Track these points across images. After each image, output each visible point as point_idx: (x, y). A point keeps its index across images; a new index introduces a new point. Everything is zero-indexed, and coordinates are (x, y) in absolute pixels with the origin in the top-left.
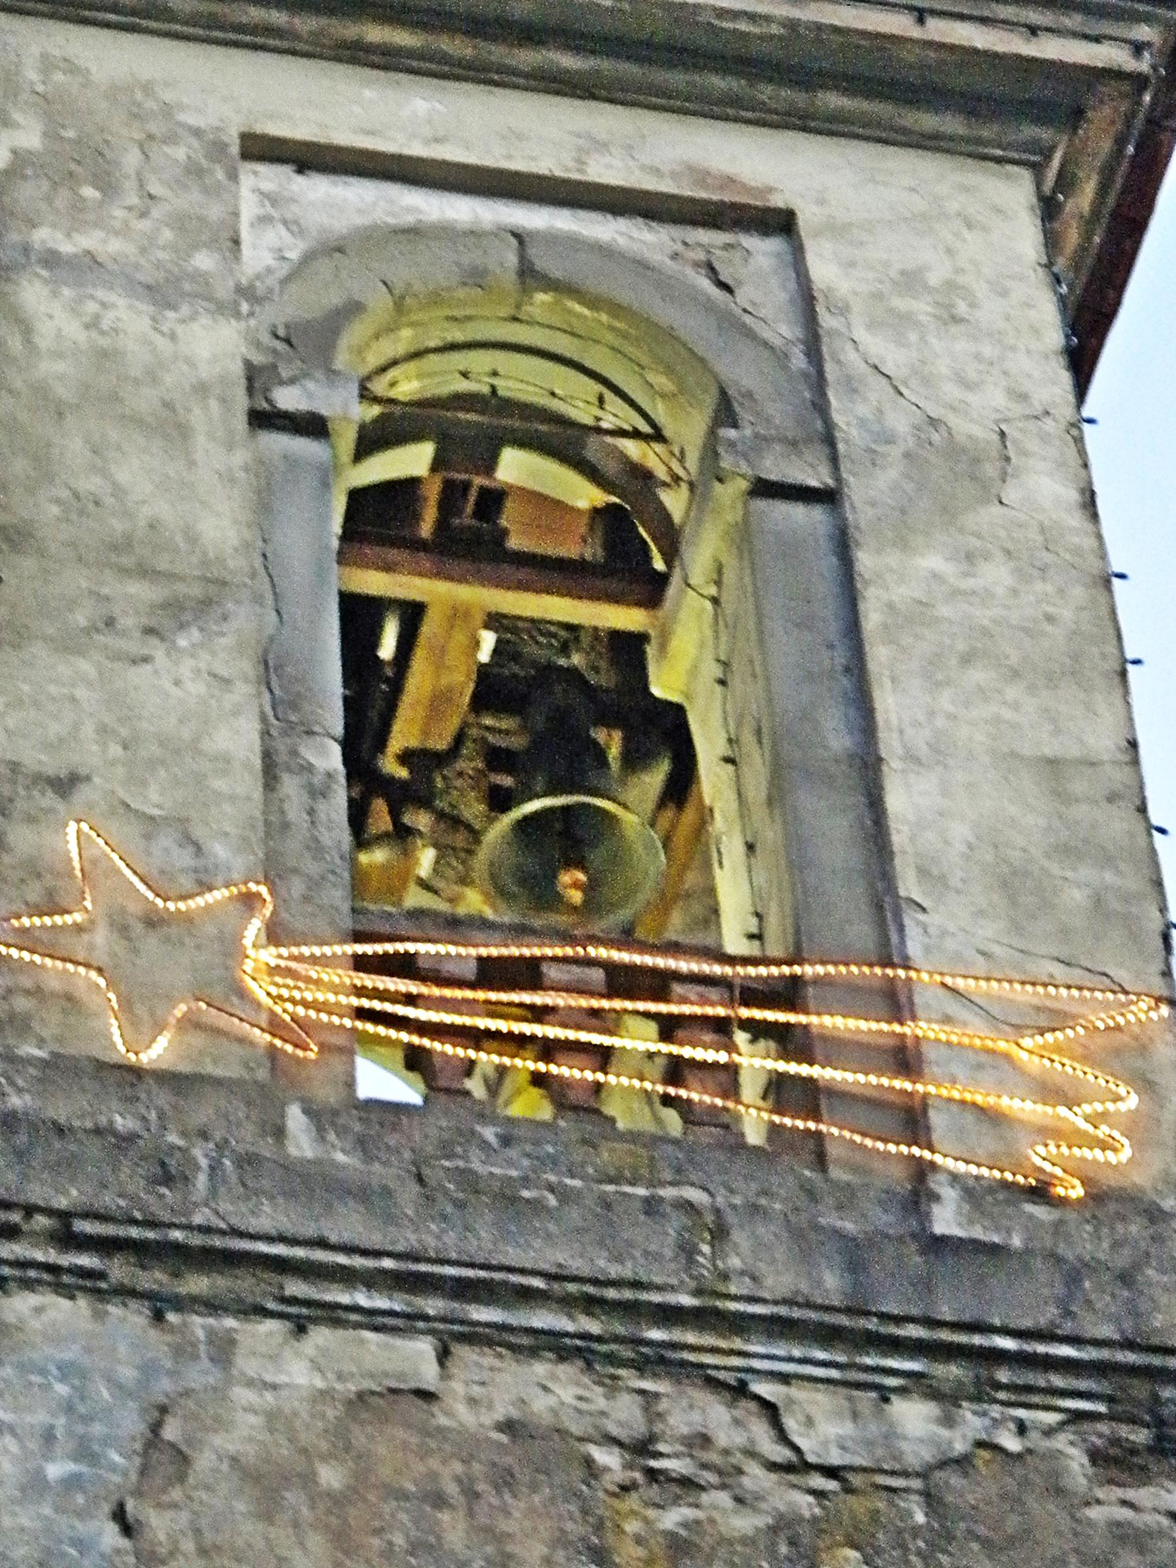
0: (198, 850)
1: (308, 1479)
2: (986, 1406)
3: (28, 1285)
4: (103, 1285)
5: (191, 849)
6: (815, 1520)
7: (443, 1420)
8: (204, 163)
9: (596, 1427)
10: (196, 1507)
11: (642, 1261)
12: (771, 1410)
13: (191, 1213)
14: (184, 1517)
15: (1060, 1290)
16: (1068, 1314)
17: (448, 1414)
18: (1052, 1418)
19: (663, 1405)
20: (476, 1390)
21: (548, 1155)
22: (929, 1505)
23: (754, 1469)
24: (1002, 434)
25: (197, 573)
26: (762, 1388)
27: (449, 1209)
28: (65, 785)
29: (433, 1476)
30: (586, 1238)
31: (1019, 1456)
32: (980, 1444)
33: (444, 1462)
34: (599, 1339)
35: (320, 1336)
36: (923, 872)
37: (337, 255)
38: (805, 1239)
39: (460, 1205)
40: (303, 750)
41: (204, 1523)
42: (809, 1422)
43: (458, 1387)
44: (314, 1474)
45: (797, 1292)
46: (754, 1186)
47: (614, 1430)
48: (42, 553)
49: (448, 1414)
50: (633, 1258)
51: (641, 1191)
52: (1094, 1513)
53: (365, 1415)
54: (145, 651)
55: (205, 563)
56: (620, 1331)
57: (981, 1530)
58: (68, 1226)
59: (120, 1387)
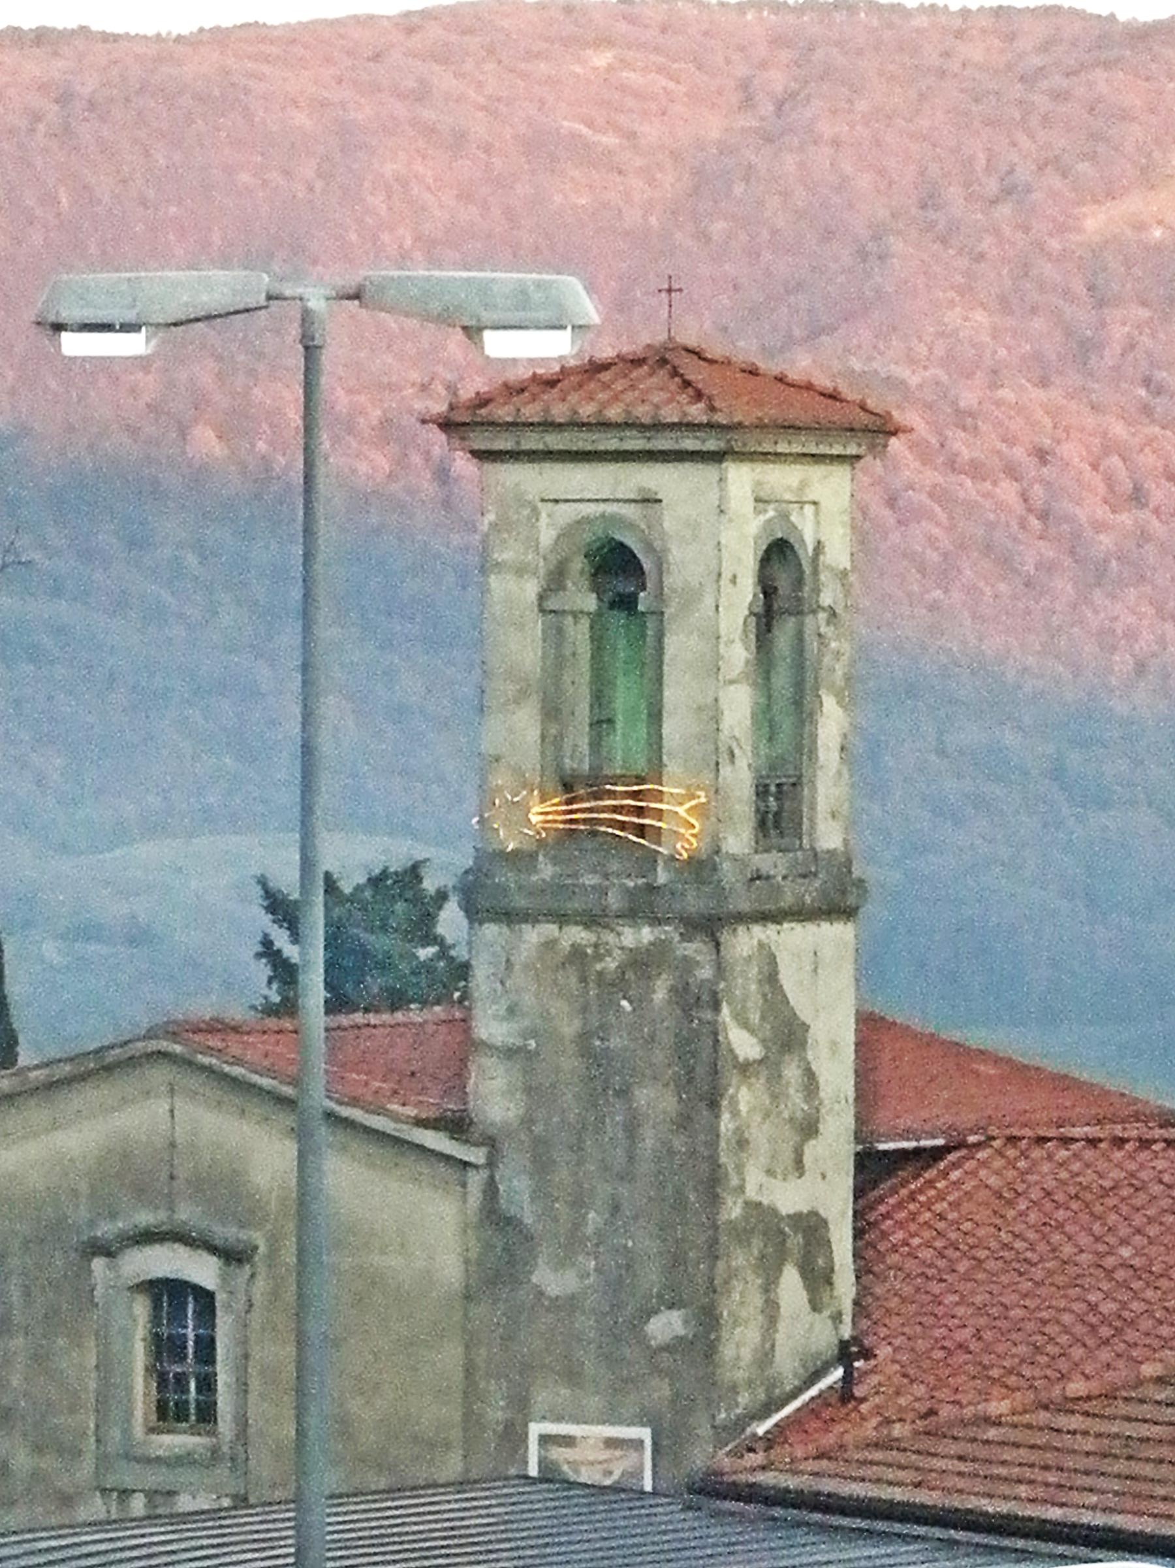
56: (591, 920)
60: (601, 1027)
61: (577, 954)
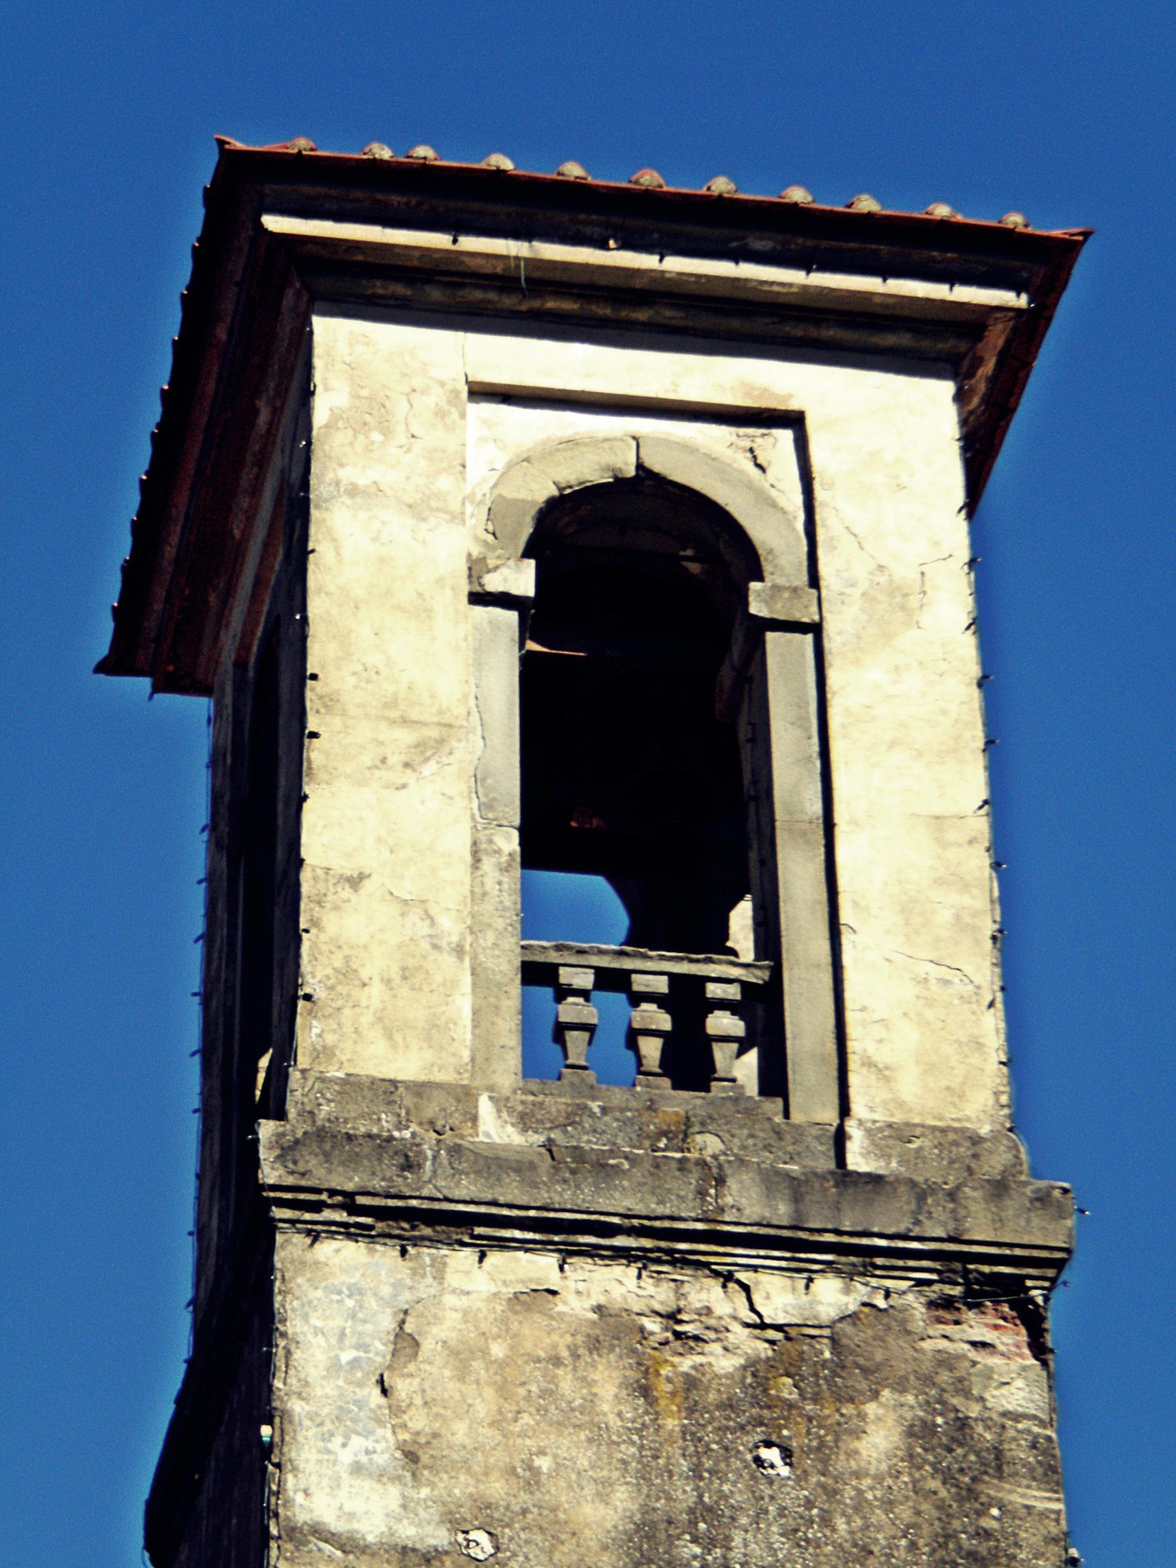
0: (433, 923)
1: (485, 1352)
2: (869, 1279)
3: (332, 1235)
4: (373, 1233)
5: (428, 922)
6: (768, 1359)
7: (561, 1308)
8: (446, 407)
9: (648, 1306)
10: (423, 1375)
11: (676, 1203)
12: (746, 1288)
13: (422, 1187)
14: (416, 1381)
15: (913, 1207)
16: (917, 1222)
17: (565, 1303)
18: (904, 1285)
19: (686, 1288)
20: (581, 1286)
21: (628, 1118)
22: (833, 1348)
23: (736, 1327)
24: (923, 574)
25: (435, 719)
26: (742, 1276)
27: (567, 1175)
28: (355, 881)
29: (555, 1346)
30: (645, 1189)
31: (885, 1310)
32: (865, 1304)
33: (561, 1336)
34: (651, 1250)
35: (495, 1258)
36: (856, 904)
37: (525, 464)
38: (772, 1180)
39: (573, 1172)
40: (496, 839)
41: (426, 1386)
42: (768, 1297)
43: (571, 1284)
44: (488, 1348)
45: (764, 1218)
46: (746, 1132)
47: (658, 1307)
48: (344, 713)
49: (565, 1303)
50: (671, 1200)
51: (678, 1155)
52: (927, 1345)
53: (518, 1308)
54: (403, 781)
55: (440, 712)
56: (662, 1246)
57: (861, 1361)
58: (354, 1201)
59: (382, 1299)
60: (703, 1511)
61: (611, 1328)
